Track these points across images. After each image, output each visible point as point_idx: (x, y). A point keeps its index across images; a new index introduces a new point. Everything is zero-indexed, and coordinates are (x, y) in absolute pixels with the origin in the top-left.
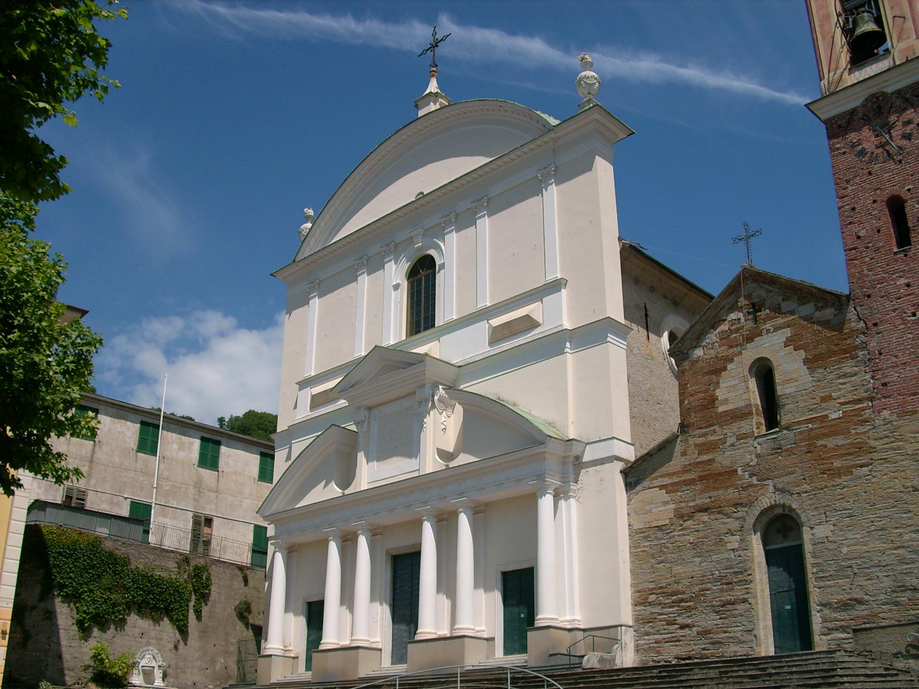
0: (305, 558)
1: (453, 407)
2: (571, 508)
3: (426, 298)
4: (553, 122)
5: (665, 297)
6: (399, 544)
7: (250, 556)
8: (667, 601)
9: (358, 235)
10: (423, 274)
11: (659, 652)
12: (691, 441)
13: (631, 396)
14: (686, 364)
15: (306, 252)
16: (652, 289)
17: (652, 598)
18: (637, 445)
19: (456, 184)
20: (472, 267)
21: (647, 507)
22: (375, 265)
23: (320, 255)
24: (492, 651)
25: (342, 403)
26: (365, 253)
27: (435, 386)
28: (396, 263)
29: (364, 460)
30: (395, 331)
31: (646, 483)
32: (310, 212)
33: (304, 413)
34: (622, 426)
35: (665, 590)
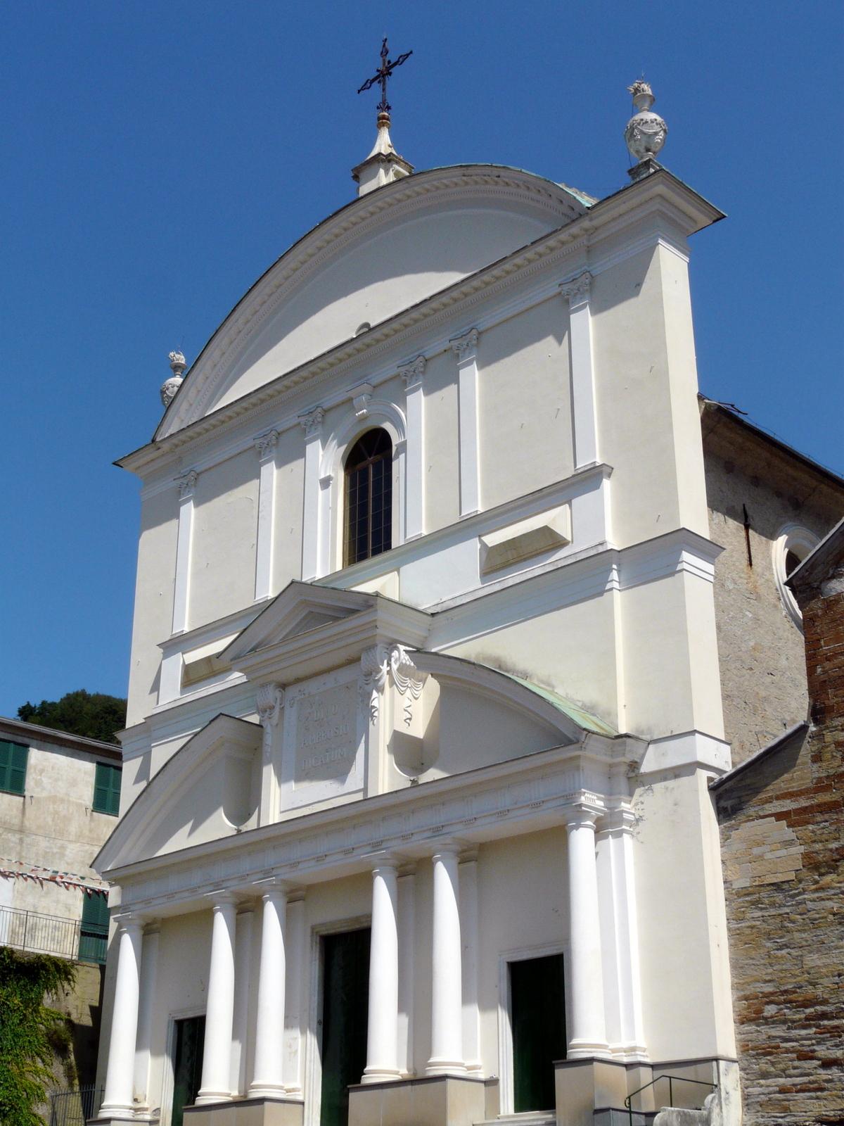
0: (174, 939)
1: (424, 681)
2: (626, 850)
3: (377, 500)
4: (587, 201)
5: (779, 494)
6: (334, 915)
7: (77, 942)
8: (797, 1017)
9: (261, 395)
10: (370, 461)
11: (786, 1110)
12: (829, 737)
13: (724, 660)
14: (817, 606)
15: (172, 426)
16: (756, 481)
17: (770, 1010)
18: (736, 744)
19: (424, 310)
20: (453, 444)
21: (756, 851)
22: (291, 452)
23: (198, 429)
24: (493, 1103)
25: (236, 677)
26: (270, 427)
27: (392, 645)
28: (324, 446)
29: (274, 780)
30: (325, 555)
31: (752, 811)
32: (181, 359)
33: (172, 694)
34: (708, 711)
35: (792, 997)
